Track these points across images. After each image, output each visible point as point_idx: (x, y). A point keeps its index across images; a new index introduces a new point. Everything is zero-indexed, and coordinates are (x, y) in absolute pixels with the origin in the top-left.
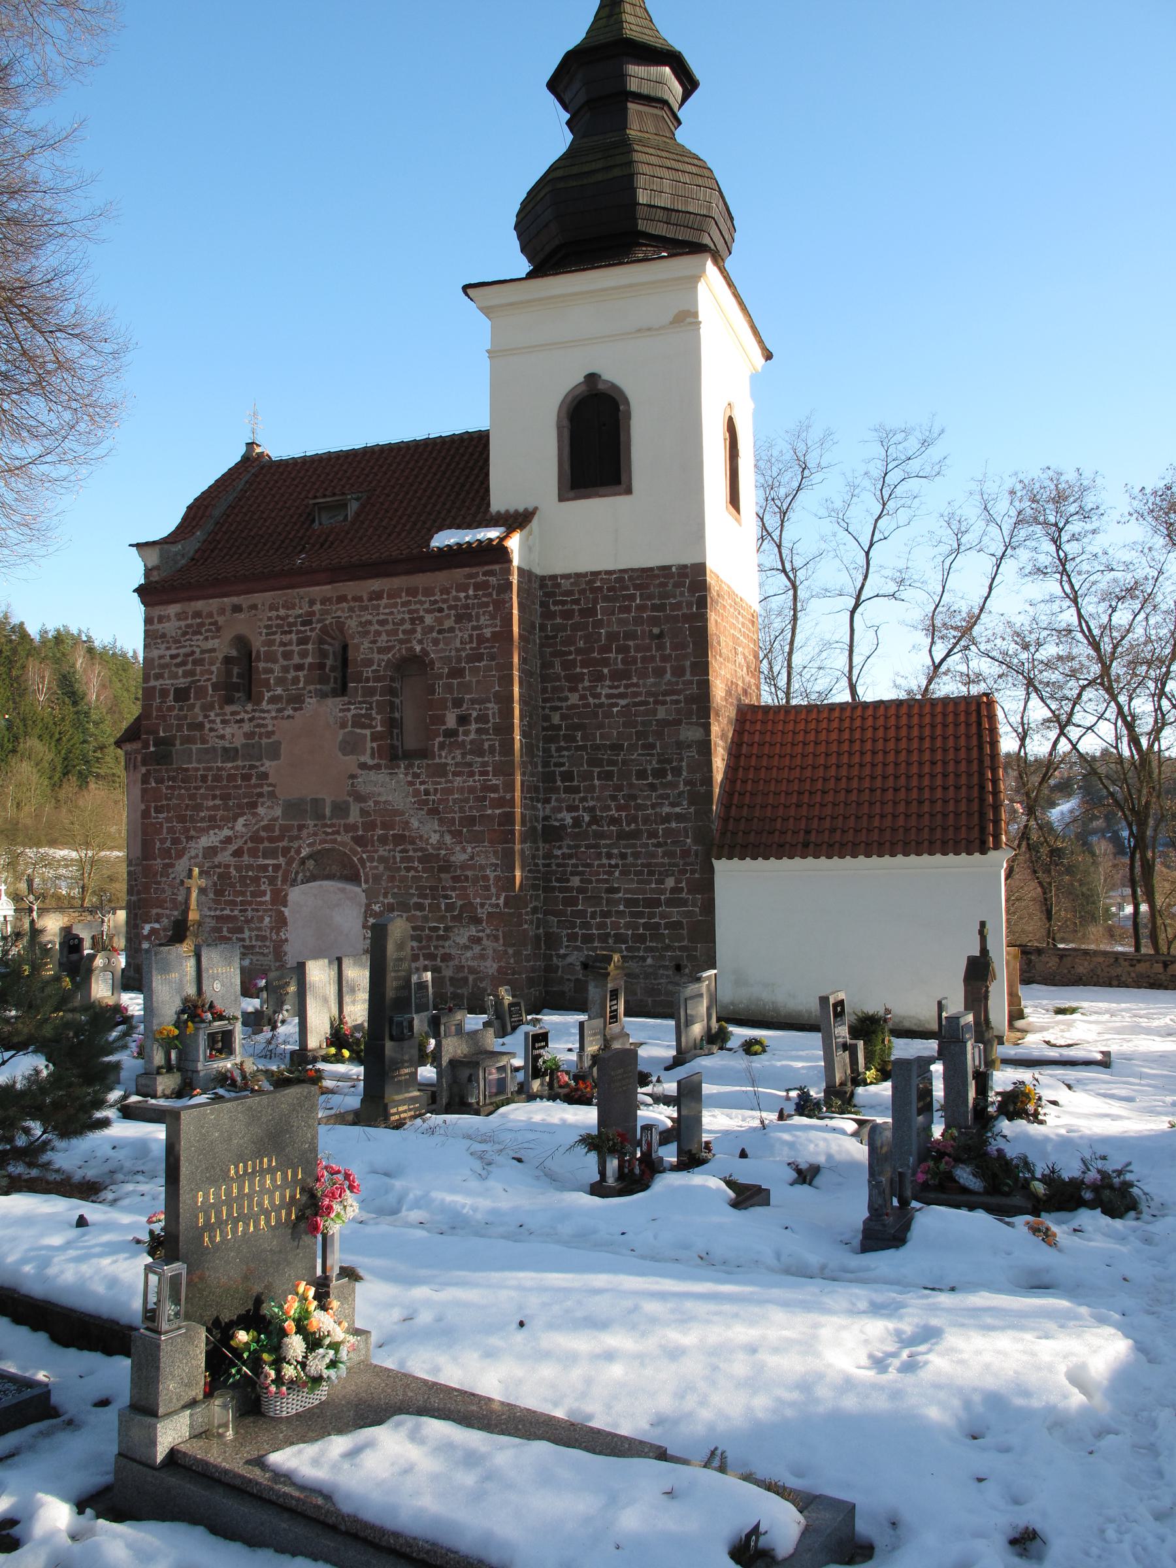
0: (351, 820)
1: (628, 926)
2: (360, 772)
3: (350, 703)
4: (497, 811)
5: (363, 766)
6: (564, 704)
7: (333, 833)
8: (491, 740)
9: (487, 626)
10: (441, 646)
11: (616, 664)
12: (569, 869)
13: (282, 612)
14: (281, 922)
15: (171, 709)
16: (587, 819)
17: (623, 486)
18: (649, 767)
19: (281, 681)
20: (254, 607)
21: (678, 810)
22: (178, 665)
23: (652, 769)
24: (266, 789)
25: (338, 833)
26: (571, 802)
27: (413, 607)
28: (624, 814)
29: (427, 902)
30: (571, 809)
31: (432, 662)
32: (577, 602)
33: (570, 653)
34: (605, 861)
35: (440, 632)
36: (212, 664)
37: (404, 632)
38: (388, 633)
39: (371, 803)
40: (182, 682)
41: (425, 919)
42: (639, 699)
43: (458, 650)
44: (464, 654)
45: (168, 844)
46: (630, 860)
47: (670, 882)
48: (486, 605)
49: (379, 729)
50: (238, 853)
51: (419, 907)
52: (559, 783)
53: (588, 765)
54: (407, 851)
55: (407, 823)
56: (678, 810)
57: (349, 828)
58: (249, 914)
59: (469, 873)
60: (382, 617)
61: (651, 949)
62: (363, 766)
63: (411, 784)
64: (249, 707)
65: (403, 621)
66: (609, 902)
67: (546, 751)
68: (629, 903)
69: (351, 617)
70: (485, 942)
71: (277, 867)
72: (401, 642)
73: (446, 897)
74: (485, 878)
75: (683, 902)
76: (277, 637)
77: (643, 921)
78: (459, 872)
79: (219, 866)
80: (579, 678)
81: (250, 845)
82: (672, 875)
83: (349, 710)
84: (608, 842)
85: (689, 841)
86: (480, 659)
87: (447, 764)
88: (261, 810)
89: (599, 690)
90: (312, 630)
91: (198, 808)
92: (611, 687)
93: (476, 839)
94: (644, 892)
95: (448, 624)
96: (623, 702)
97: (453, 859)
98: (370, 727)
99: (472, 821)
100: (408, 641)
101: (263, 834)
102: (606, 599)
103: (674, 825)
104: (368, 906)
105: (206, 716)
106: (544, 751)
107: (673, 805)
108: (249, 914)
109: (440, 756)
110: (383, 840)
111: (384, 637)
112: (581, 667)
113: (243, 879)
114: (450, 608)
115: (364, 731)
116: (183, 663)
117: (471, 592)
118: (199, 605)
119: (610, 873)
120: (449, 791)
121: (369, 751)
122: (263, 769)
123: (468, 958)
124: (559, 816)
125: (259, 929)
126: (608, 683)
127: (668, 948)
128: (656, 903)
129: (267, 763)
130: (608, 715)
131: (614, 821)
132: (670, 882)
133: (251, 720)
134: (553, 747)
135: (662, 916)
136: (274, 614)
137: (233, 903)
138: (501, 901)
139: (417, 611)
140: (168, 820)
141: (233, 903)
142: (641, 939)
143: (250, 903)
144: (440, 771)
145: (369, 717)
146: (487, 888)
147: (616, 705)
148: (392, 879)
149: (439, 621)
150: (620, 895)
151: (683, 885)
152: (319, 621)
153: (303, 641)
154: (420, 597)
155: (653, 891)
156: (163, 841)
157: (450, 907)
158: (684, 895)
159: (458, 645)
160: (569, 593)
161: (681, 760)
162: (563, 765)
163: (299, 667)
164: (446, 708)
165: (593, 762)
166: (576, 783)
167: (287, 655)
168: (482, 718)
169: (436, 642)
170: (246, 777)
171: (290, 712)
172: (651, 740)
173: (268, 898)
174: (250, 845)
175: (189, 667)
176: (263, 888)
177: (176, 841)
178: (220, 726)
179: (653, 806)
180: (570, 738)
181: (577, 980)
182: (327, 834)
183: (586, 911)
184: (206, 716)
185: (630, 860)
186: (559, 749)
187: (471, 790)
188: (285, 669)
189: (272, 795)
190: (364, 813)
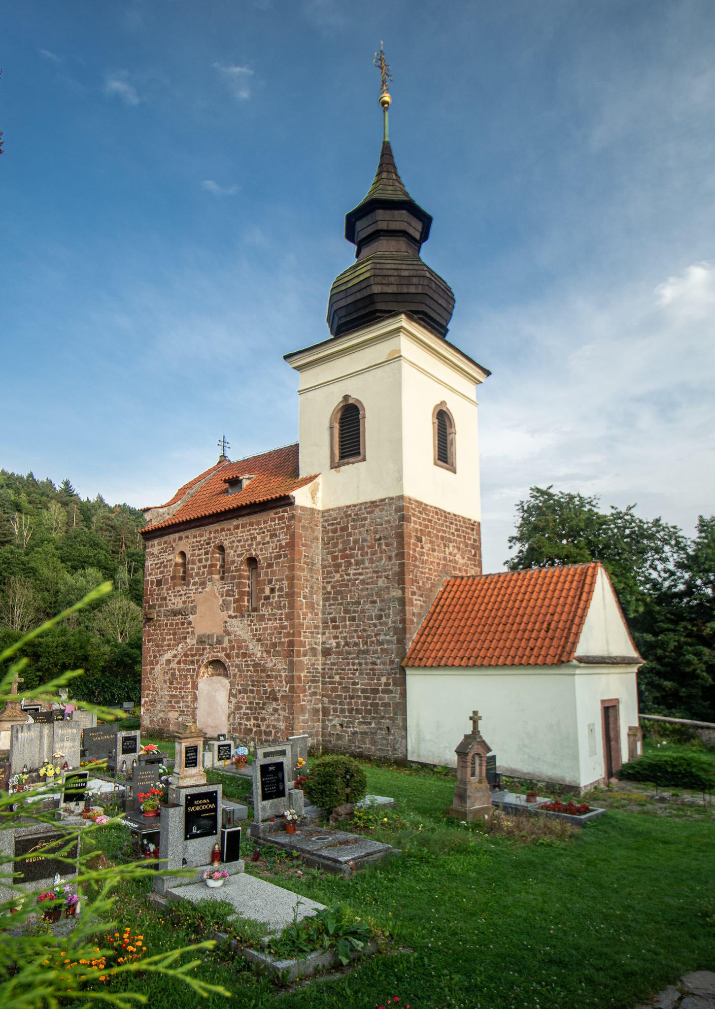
0: (224, 645)
1: (362, 704)
2: (228, 620)
3: (225, 584)
4: (287, 640)
5: (230, 617)
6: (333, 580)
7: (217, 652)
8: (285, 602)
9: (283, 539)
10: (264, 552)
11: (357, 556)
12: (334, 671)
13: (198, 539)
14: (195, 698)
15: (154, 590)
16: (343, 643)
17: (361, 458)
18: (374, 614)
19: (197, 574)
20: (187, 537)
22: (158, 568)
23: (376, 615)
24: (190, 630)
25: (219, 652)
26: (335, 634)
27: (252, 532)
28: (361, 640)
29: (255, 689)
30: (336, 637)
31: (260, 561)
32: (339, 523)
33: (335, 552)
34: (351, 667)
35: (264, 544)
36: (171, 567)
37: (248, 545)
38: (242, 546)
39: (233, 636)
40: (160, 576)
41: (254, 698)
43: (271, 553)
44: (273, 555)
45: (152, 658)
46: (364, 666)
47: (384, 680)
48: (283, 528)
49: (237, 597)
50: (179, 663)
51: (252, 691)
52: (330, 623)
53: (344, 613)
54: (247, 661)
55: (248, 646)
57: (224, 649)
58: (183, 693)
59: (274, 673)
60: (239, 538)
61: (374, 718)
62: (230, 617)
63: (250, 625)
64: (185, 588)
65: (247, 540)
66: (354, 690)
67: (324, 605)
68: (363, 691)
69: (226, 539)
70: (280, 712)
71: (194, 670)
72: (247, 551)
73: (264, 686)
74: (281, 676)
75: (391, 692)
76: (196, 552)
77: (370, 702)
78: (269, 673)
79: (171, 669)
80: (339, 565)
81: (184, 658)
83: (224, 587)
86: (280, 558)
87: (264, 615)
88: (188, 641)
89: (349, 572)
90: (210, 547)
91: (164, 640)
92: (355, 570)
93: (276, 654)
94: (370, 685)
95: (267, 539)
96: (361, 577)
97: (267, 665)
98: (233, 596)
99: (274, 645)
100: (250, 550)
101: (189, 653)
102: (354, 520)
103: (386, 646)
104: (231, 690)
105: (168, 594)
106: (323, 606)
107: (385, 635)
108: (183, 693)
110: (237, 656)
111: (240, 548)
112: (341, 559)
113: (181, 675)
114: (268, 531)
115: (230, 598)
116: (160, 568)
117: (277, 522)
118: (166, 538)
119: (354, 674)
120: (265, 629)
121: (232, 609)
122: (189, 619)
123: (272, 720)
124: (330, 642)
125: (186, 702)
127: (383, 718)
128: (376, 691)
129: (191, 616)
130: (354, 585)
131: (356, 644)
132: (384, 680)
133: (185, 594)
134: (327, 604)
135: (380, 700)
136: (195, 540)
137: (176, 688)
138: (287, 689)
139: (253, 534)
140: (153, 646)
141: (176, 688)
142: (368, 712)
143: (183, 688)
144: (261, 618)
145: (232, 590)
146: (281, 682)
147: (357, 579)
148: (240, 676)
149: (263, 538)
150: (359, 686)
151: (391, 681)
152: (213, 542)
153: (206, 553)
154: (255, 526)
155: (375, 684)
156: (150, 656)
157: (265, 692)
158: (391, 687)
159: (271, 551)
160: (335, 519)
161: (389, 609)
162: (331, 613)
163: (205, 567)
164: (265, 585)
165: (346, 611)
166: (337, 623)
167: (200, 561)
168: (281, 589)
169: (261, 550)
170: (183, 624)
171: (200, 590)
173: (190, 686)
174: (184, 658)
175: (162, 569)
176: (188, 680)
177: (155, 657)
178: (173, 598)
179: (376, 635)
180: (335, 599)
181: (337, 734)
182: (214, 652)
183: (342, 695)
184: (168, 594)
185: (364, 666)
186: (330, 605)
187: (275, 628)
188: (199, 568)
189: (193, 632)
190: (230, 641)
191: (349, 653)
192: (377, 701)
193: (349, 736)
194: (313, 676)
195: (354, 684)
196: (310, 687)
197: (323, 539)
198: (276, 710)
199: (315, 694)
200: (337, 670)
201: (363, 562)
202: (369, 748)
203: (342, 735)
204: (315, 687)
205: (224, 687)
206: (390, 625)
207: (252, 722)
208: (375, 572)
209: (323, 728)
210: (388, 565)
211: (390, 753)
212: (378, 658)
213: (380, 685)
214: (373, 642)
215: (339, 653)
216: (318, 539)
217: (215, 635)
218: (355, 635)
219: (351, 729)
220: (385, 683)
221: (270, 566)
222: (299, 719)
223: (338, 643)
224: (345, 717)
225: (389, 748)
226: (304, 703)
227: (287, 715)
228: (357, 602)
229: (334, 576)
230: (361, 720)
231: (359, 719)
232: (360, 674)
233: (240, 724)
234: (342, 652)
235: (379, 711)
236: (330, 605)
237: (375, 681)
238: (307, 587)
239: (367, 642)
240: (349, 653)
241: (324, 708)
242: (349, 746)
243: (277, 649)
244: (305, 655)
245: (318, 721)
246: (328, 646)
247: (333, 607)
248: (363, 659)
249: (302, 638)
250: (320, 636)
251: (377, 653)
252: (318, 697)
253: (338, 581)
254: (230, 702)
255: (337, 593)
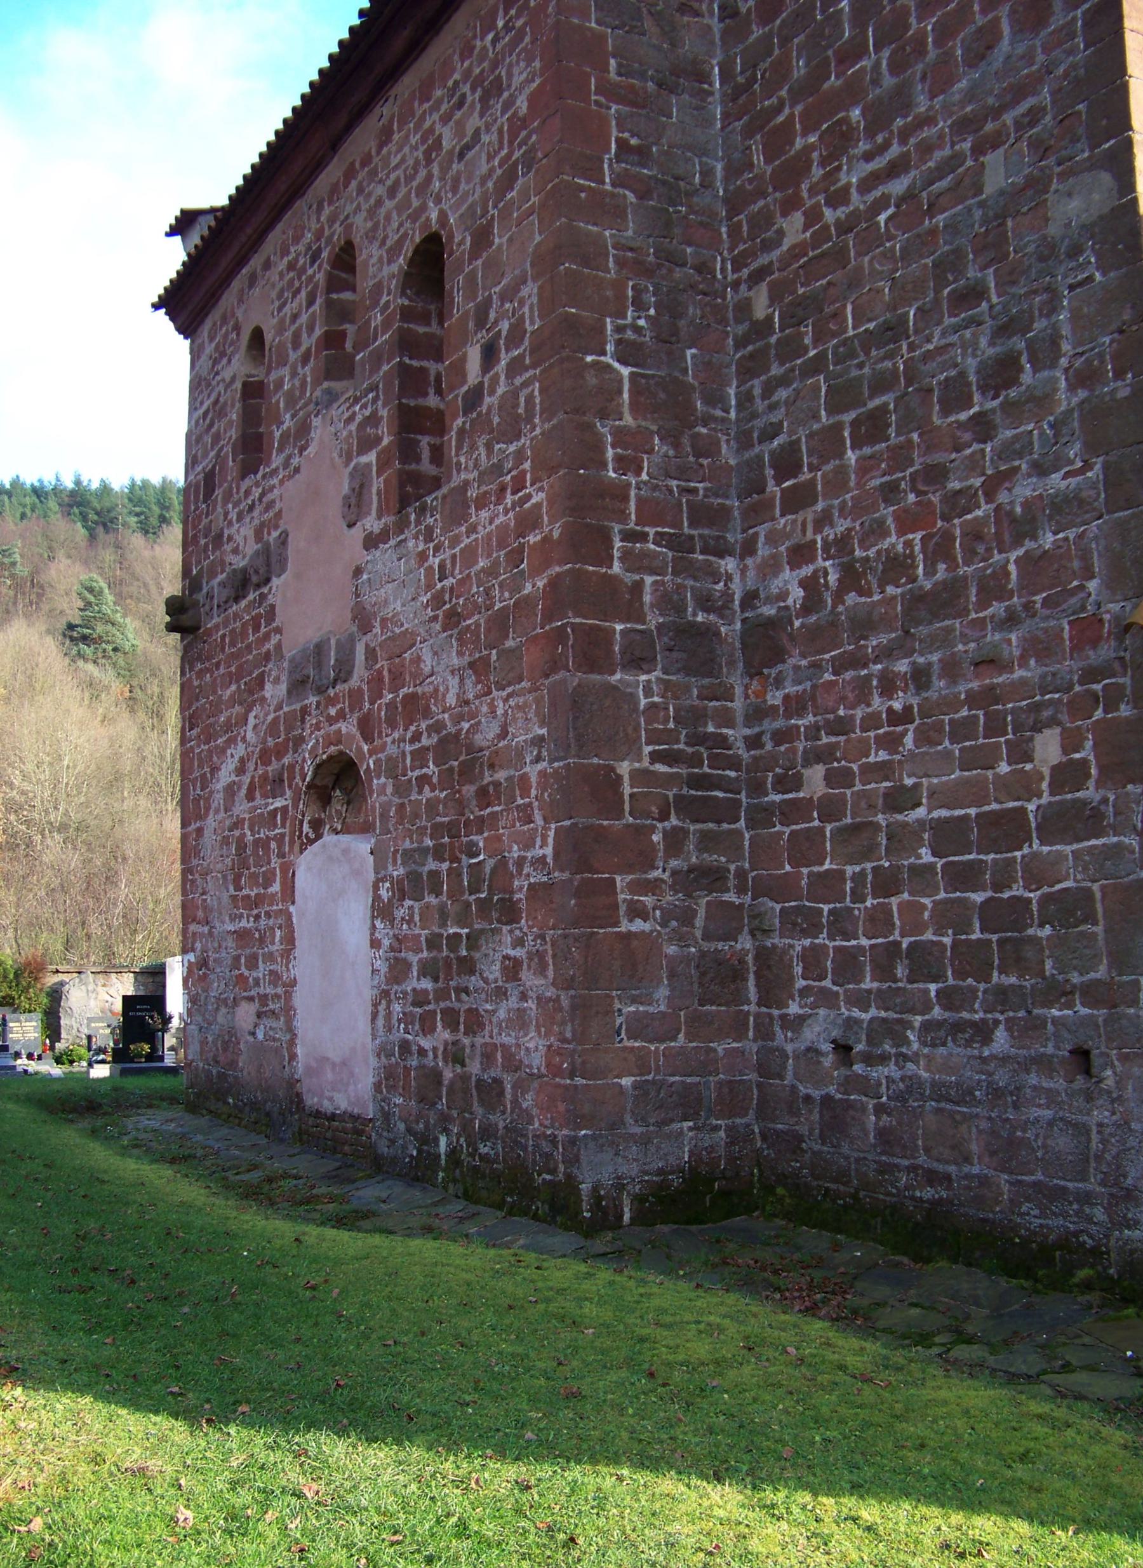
6: (775, 254)
12: (800, 745)
16: (833, 578)
18: (971, 363)
21: (1056, 481)
30: (801, 554)
33: (779, 109)
34: (877, 702)
42: (938, 155)
56: (1056, 481)
61: (1002, 997)
62: (371, 542)
66: (902, 839)
77: (978, 897)
82: (1053, 722)
84: (884, 639)
85: (1092, 585)
92: (868, 157)
96: (898, 187)
103: (1048, 540)
109: (496, 981)
119: (892, 743)
120: (469, 555)
126: (863, 146)
127: (1058, 993)
130: (871, 240)
135: (1034, 879)
147: (881, 204)
151: (1086, 752)
155: (1005, 786)
158: (1090, 793)
161: (1052, 307)
172: (972, 273)
179: (990, 489)
180: (790, 348)
181: (827, 1100)
191: (863, 625)
192: (1017, 890)
193: (880, 1110)
194: (698, 782)
195: (900, 800)
196: (674, 842)
197: (727, 74)
198: (512, 969)
199: (713, 878)
200: (813, 732)
201: (901, 100)
202: (984, 1181)
203: (849, 1105)
204: (707, 841)
205: (357, 873)
206: (1065, 399)
207: (443, 1034)
208: (963, 126)
209: (763, 1069)
210: (1029, 58)
211: (1099, 1214)
212: (1011, 620)
213: (1026, 787)
214: (974, 535)
215: (818, 638)
216: (703, 77)
217: (333, 642)
218: (887, 512)
219: (891, 1070)
220: (1057, 770)
221: (482, 238)
222: (609, 1012)
223: (810, 585)
224: (861, 1000)
225: (1092, 1184)
226: (638, 925)
227: (550, 993)
228: (887, 327)
229: (781, 233)
230: (937, 1012)
231: (927, 1008)
232: (923, 738)
233: (405, 1046)
234: (833, 624)
235: (1029, 953)
236: (768, 392)
237: (1004, 768)
238: (640, 305)
239: (948, 537)
240: (863, 625)
241: (763, 956)
242: (885, 1169)
243: (510, 643)
244: (638, 661)
245: (738, 1028)
246: (769, 611)
247: (782, 394)
248: (932, 643)
249: (617, 568)
250: (729, 564)
251: (1003, 594)
252: (731, 897)
253: (798, 251)
254: (375, 944)
255: (792, 319)
